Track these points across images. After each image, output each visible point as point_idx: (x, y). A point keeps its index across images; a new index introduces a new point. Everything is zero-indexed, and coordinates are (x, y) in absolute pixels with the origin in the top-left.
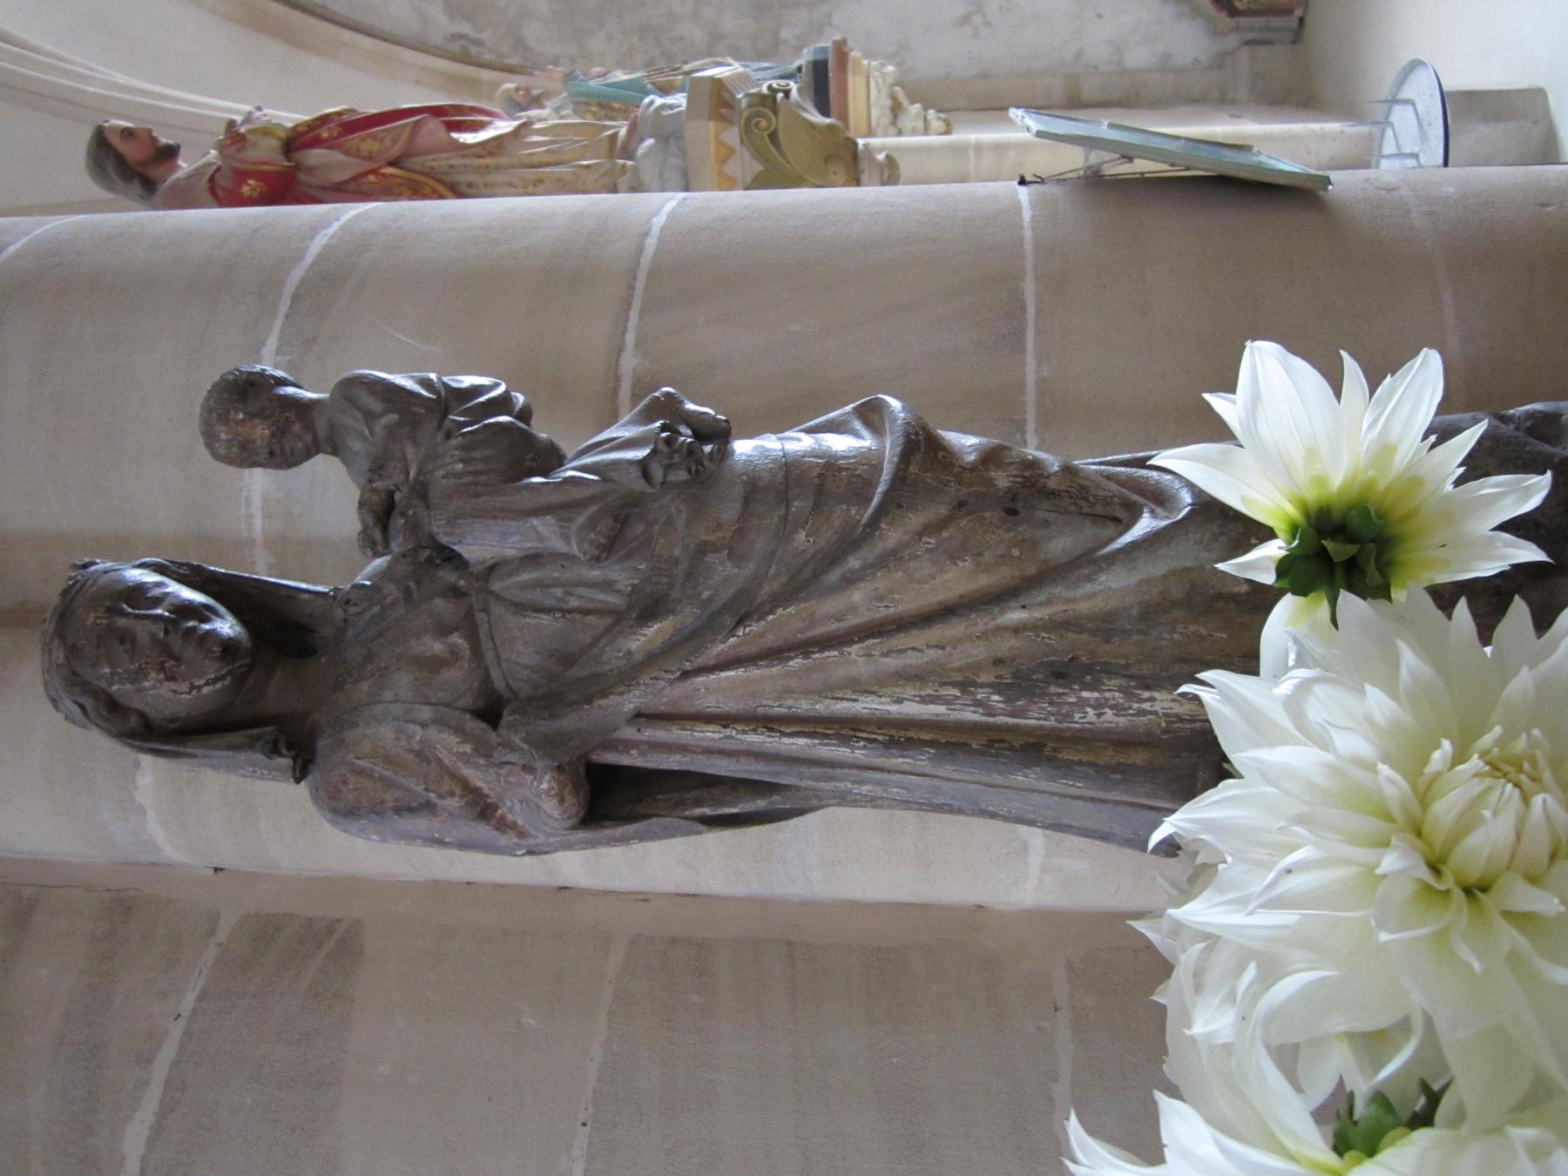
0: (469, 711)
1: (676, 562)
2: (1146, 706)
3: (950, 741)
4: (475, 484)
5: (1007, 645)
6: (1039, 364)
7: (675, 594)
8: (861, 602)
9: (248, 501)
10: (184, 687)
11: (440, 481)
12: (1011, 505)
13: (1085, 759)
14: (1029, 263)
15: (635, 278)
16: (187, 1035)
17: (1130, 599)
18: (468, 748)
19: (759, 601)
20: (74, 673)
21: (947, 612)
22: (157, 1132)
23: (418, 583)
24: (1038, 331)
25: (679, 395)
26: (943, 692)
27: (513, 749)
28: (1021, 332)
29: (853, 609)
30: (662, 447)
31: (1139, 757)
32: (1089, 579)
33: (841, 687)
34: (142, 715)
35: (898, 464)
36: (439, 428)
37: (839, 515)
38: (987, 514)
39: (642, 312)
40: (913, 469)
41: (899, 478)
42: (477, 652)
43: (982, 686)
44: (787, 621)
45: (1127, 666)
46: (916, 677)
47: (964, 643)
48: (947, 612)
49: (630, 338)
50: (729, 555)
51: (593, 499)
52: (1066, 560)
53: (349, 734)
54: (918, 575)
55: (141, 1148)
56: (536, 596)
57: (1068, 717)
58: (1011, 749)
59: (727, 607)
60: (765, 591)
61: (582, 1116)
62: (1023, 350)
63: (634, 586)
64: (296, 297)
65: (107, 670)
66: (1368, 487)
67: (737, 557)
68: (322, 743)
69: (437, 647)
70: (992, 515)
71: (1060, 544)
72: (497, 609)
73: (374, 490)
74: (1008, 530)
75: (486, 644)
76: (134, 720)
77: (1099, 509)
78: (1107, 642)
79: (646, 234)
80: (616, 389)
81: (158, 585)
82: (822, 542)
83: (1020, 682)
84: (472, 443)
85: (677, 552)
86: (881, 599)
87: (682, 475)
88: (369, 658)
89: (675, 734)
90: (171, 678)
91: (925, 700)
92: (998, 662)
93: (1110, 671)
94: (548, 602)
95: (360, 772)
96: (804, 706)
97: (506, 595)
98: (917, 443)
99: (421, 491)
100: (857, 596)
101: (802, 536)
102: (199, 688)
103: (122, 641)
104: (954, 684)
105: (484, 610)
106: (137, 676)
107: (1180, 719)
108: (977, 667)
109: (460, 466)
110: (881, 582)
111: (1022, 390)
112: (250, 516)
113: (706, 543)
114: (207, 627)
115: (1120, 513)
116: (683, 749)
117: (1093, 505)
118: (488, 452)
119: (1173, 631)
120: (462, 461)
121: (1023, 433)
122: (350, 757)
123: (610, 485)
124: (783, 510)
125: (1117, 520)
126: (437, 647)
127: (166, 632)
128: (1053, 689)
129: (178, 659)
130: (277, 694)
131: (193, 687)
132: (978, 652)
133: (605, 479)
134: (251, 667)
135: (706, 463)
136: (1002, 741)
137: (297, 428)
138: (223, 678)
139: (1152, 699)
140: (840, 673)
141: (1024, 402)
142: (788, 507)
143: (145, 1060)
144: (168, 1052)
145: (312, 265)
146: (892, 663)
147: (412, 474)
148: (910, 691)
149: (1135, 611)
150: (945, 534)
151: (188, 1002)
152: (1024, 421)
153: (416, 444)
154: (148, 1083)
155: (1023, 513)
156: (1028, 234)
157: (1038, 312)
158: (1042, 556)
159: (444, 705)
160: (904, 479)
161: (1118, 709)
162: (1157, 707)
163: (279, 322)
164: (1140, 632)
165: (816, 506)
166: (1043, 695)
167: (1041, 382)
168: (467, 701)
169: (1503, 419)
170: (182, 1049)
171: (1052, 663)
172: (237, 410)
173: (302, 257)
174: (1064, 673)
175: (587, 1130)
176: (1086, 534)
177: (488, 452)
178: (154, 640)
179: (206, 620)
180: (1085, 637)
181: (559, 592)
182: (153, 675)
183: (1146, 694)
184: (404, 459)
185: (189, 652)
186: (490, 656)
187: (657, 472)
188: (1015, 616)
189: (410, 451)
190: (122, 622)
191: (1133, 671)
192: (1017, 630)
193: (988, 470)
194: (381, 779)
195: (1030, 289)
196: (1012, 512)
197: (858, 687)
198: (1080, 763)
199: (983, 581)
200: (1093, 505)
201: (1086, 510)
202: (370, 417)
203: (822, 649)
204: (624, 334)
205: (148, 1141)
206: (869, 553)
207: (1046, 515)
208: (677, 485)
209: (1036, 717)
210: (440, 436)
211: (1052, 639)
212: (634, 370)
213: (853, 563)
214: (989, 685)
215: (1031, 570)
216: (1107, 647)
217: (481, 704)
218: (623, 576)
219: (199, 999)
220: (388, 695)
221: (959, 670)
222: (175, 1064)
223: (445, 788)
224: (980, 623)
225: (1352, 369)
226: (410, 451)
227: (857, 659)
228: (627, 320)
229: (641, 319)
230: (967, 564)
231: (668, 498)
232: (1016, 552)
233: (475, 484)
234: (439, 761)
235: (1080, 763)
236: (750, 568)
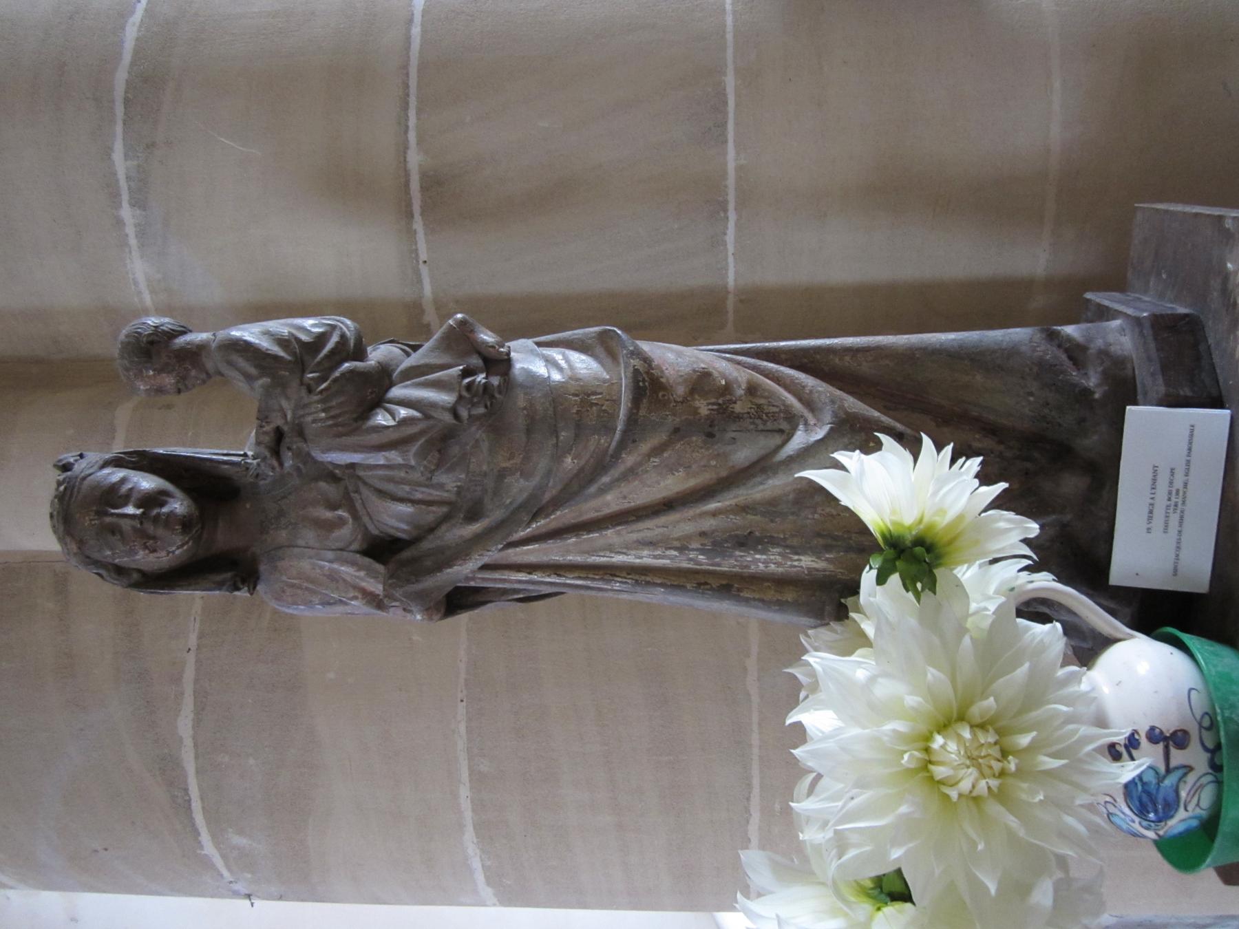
0: (358, 552)
1: (485, 475)
2: (796, 563)
3: (674, 579)
4: (336, 425)
5: (709, 524)
6: (738, 153)
7: (487, 500)
8: (612, 502)
9: (136, 283)
10: (164, 553)
11: (311, 429)
12: (710, 430)
13: (757, 596)
14: (729, 37)
15: (407, 75)
16: (198, 662)
17: (789, 488)
18: (362, 574)
19: (544, 501)
20: (88, 557)
21: (667, 505)
22: (197, 722)
23: (305, 464)
24: (736, 124)
25: (471, 320)
26: (668, 553)
27: (396, 600)
28: (724, 125)
29: (608, 504)
30: (465, 393)
31: (789, 596)
32: (761, 483)
33: (604, 550)
34: (139, 571)
35: (631, 409)
36: (302, 384)
37: (596, 442)
38: (694, 439)
39: (419, 111)
40: (642, 412)
41: (632, 420)
42: (356, 516)
43: (693, 550)
44: (563, 516)
45: (785, 539)
46: (651, 544)
47: (681, 524)
48: (667, 505)
49: (412, 136)
50: (521, 475)
51: (422, 433)
52: (747, 464)
53: (279, 564)
54: (648, 482)
55: (191, 732)
56: (390, 487)
57: (747, 567)
58: (712, 589)
59: (523, 506)
60: (547, 496)
61: (460, 696)
62: (726, 142)
63: (458, 487)
64: (127, 102)
65: (109, 553)
66: (930, 527)
67: (526, 475)
68: (263, 568)
69: (329, 515)
70: (697, 439)
71: (743, 454)
72: (365, 492)
73: (266, 433)
74: (708, 449)
75: (361, 511)
76: (135, 576)
77: (770, 425)
78: (772, 521)
79: (410, 21)
80: (407, 184)
81: (123, 481)
82: (583, 462)
83: (718, 544)
84: (327, 396)
85: (485, 468)
86: (625, 498)
87: (481, 410)
88: (281, 514)
89: (497, 575)
90: (154, 551)
91: (655, 557)
92: (703, 534)
93: (773, 541)
94: (400, 494)
95: (293, 586)
96: (579, 559)
97: (370, 481)
98: (644, 388)
99: (300, 432)
100: (609, 497)
101: (569, 460)
102: (173, 552)
103: (113, 533)
104: (676, 549)
105: (356, 492)
106: (132, 552)
107: (817, 570)
108: (688, 538)
109: (323, 415)
110: (625, 488)
111: (724, 175)
112: (140, 293)
113: (504, 469)
114: (165, 510)
115: (784, 425)
116: (505, 581)
117: (765, 422)
118: (342, 399)
119: (815, 512)
120: (323, 410)
121: (726, 211)
122: (284, 578)
123: (432, 422)
124: (554, 441)
125: (781, 431)
126: (329, 515)
127: (141, 523)
128: (738, 553)
129: (154, 538)
130: (224, 538)
131: (169, 553)
132: (688, 528)
133: (427, 417)
134: (203, 528)
135: (497, 396)
136: (706, 583)
137: (193, 373)
138: (187, 542)
139: (799, 560)
140: (601, 542)
141: (726, 186)
142: (557, 437)
143: (177, 680)
144: (189, 674)
145: (133, 64)
146: (635, 536)
147: (289, 417)
148: (645, 553)
149: (791, 497)
150: (665, 455)
151: (193, 640)
152: (726, 202)
153: (288, 398)
154: (183, 694)
155: (718, 436)
156: (729, 20)
157: (737, 105)
158: (731, 464)
159: (341, 550)
160: (636, 421)
161: (778, 564)
162: (803, 564)
163: (119, 129)
164: (793, 513)
165: (577, 436)
166: (731, 556)
167: (739, 169)
168: (355, 546)
169: (1052, 336)
170: (197, 670)
171: (737, 536)
172: (147, 369)
173: (118, 56)
174: (745, 542)
175: (464, 704)
176: (763, 444)
177: (342, 399)
178: (134, 527)
179: (162, 504)
180: (758, 518)
181: (407, 488)
182: (141, 552)
183: (796, 557)
184: (282, 410)
185: (160, 532)
186: (366, 519)
187: (464, 413)
188: (713, 506)
189: (285, 404)
190: (108, 520)
191: (788, 542)
192: (714, 514)
193: (694, 400)
194: (307, 589)
195: (730, 81)
196: (710, 435)
197: (611, 548)
198: (754, 599)
199: (692, 483)
200: (765, 422)
201: (761, 427)
202: (249, 378)
203: (589, 532)
204: (406, 132)
205: (193, 727)
206: (615, 472)
207: (733, 435)
208: (478, 417)
209: (727, 565)
210: (304, 392)
211: (737, 520)
212: (420, 165)
213: (606, 479)
214: (697, 550)
215: (724, 474)
216: (772, 525)
217: (365, 546)
218: (449, 482)
219: (200, 637)
220: (301, 542)
221: (678, 539)
222: (196, 681)
223: (351, 595)
224: (691, 512)
225: (927, 442)
226: (285, 404)
227: (610, 535)
228: (407, 119)
229: (418, 119)
230: (681, 473)
231: (473, 429)
232: (713, 463)
233: (336, 425)
234: (344, 580)
235: (754, 599)
236: (535, 481)
